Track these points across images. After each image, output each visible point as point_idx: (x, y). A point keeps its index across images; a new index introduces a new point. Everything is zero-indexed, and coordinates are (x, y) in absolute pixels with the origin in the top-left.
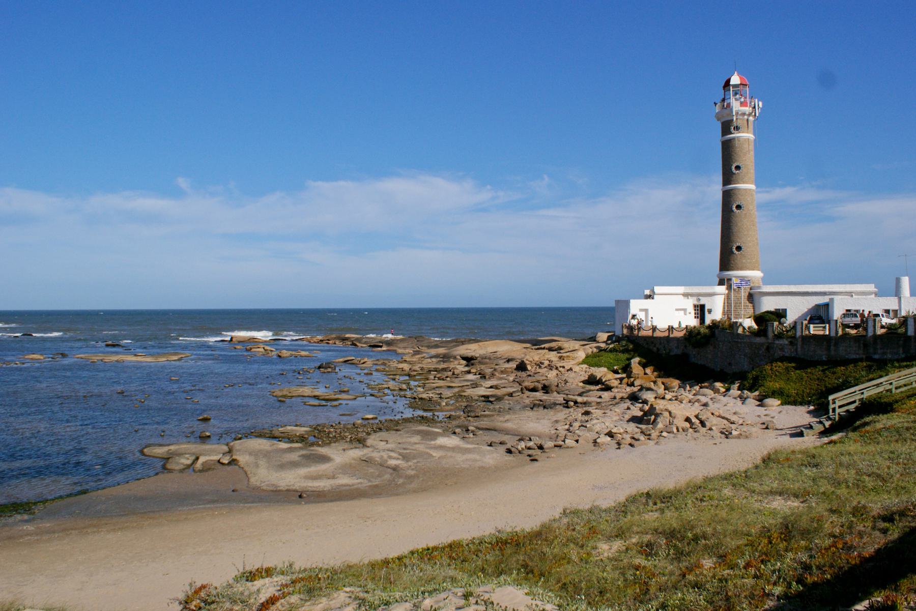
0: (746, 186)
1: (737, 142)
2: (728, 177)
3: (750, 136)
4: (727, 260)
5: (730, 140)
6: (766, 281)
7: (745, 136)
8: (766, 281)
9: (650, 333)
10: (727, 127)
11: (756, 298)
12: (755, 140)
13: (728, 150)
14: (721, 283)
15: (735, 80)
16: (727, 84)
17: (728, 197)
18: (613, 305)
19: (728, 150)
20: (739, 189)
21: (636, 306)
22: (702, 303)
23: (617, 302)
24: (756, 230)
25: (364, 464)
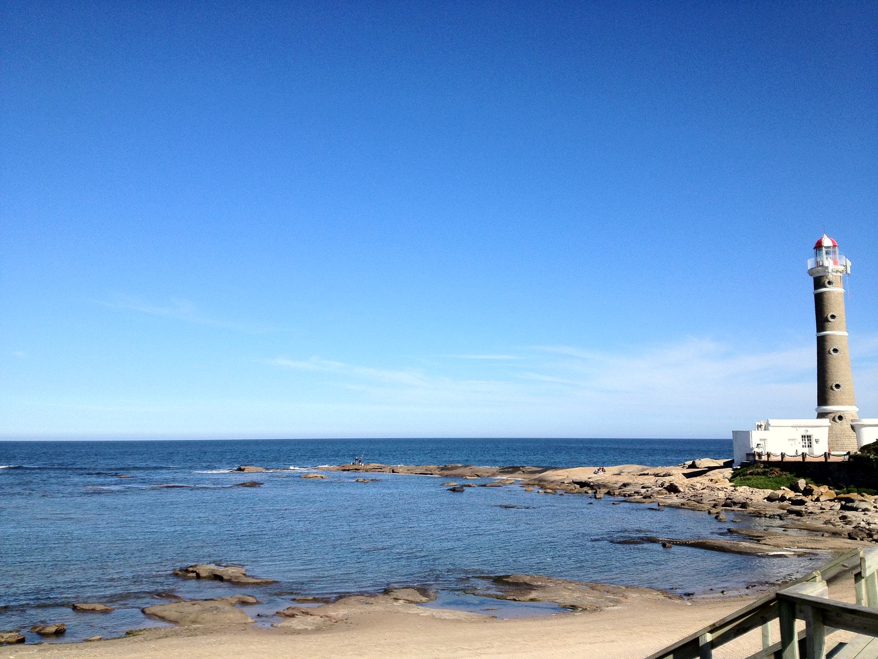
0: (837, 333)
1: (825, 296)
2: (822, 321)
3: (841, 290)
4: (823, 398)
5: (822, 294)
6: (862, 414)
7: (835, 291)
8: (862, 414)
9: (779, 459)
10: (819, 282)
11: (856, 429)
12: (845, 294)
13: (820, 301)
14: (821, 415)
15: (827, 242)
16: (819, 246)
17: (822, 342)
18: (730, 436)
19: (820, 301)
20: (829, 335)
21: (756, 437)
22: (809, 434)
23: (735, 433)
24: (842, 369)
25: (853, 536)
